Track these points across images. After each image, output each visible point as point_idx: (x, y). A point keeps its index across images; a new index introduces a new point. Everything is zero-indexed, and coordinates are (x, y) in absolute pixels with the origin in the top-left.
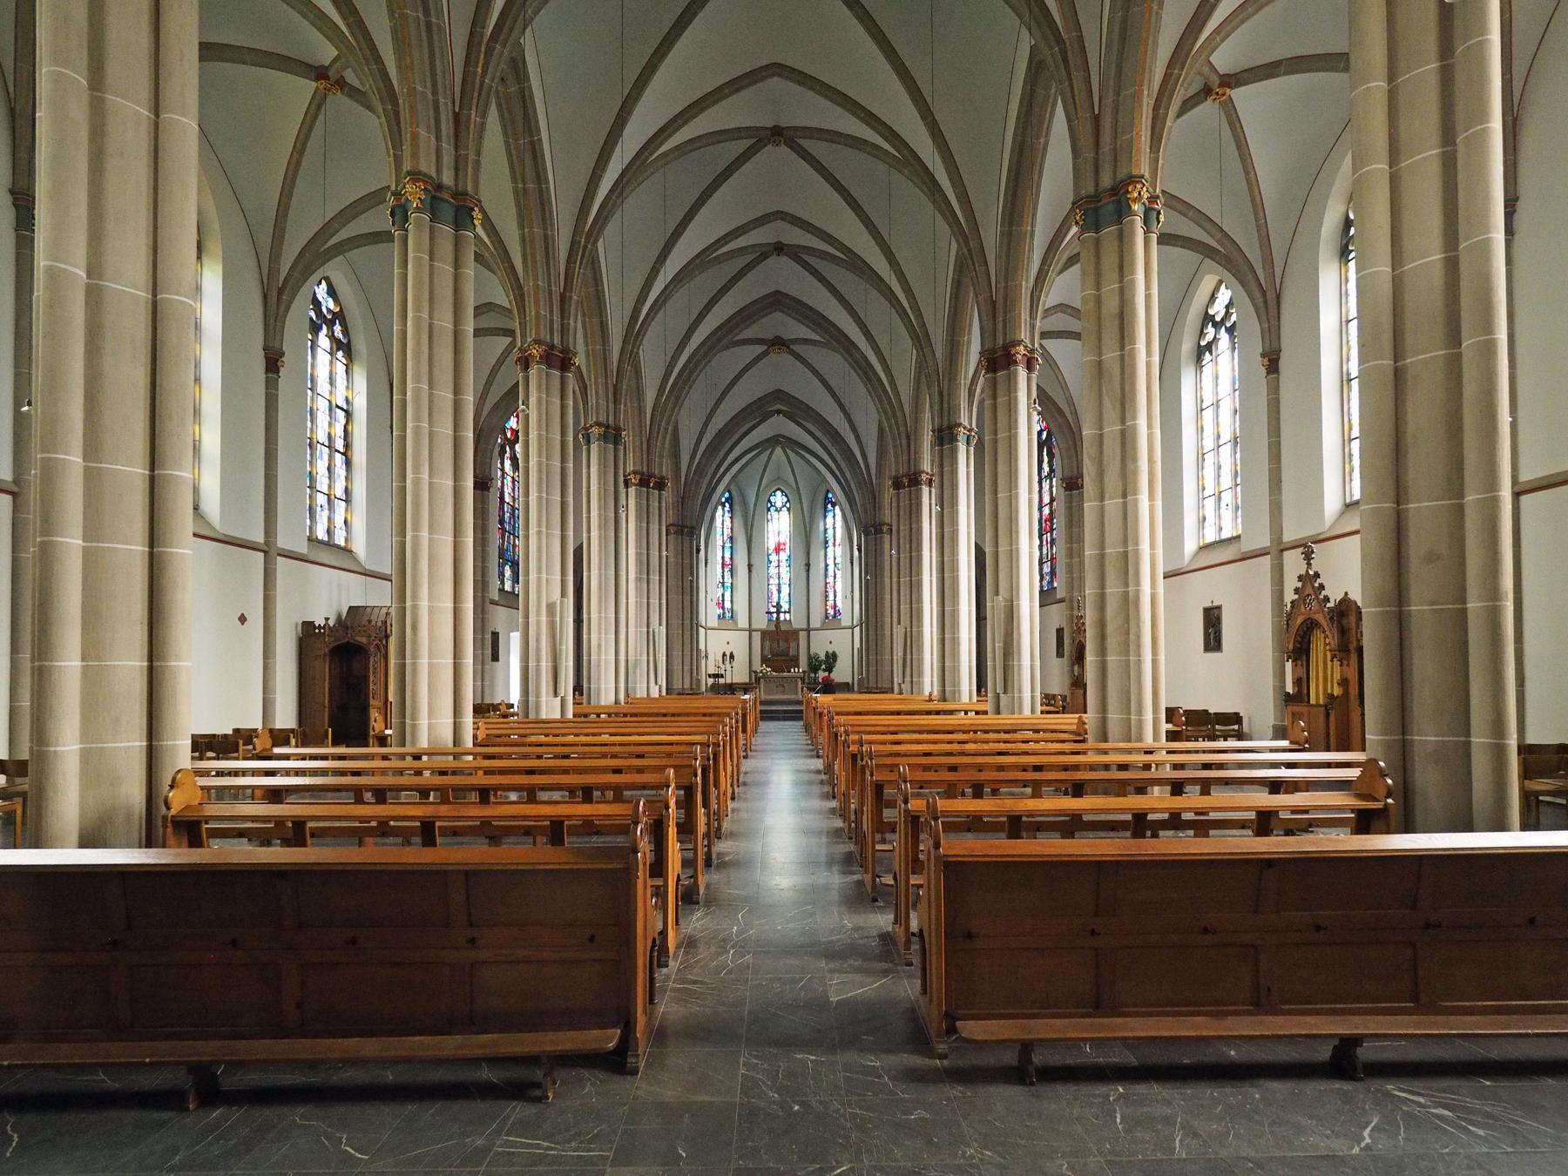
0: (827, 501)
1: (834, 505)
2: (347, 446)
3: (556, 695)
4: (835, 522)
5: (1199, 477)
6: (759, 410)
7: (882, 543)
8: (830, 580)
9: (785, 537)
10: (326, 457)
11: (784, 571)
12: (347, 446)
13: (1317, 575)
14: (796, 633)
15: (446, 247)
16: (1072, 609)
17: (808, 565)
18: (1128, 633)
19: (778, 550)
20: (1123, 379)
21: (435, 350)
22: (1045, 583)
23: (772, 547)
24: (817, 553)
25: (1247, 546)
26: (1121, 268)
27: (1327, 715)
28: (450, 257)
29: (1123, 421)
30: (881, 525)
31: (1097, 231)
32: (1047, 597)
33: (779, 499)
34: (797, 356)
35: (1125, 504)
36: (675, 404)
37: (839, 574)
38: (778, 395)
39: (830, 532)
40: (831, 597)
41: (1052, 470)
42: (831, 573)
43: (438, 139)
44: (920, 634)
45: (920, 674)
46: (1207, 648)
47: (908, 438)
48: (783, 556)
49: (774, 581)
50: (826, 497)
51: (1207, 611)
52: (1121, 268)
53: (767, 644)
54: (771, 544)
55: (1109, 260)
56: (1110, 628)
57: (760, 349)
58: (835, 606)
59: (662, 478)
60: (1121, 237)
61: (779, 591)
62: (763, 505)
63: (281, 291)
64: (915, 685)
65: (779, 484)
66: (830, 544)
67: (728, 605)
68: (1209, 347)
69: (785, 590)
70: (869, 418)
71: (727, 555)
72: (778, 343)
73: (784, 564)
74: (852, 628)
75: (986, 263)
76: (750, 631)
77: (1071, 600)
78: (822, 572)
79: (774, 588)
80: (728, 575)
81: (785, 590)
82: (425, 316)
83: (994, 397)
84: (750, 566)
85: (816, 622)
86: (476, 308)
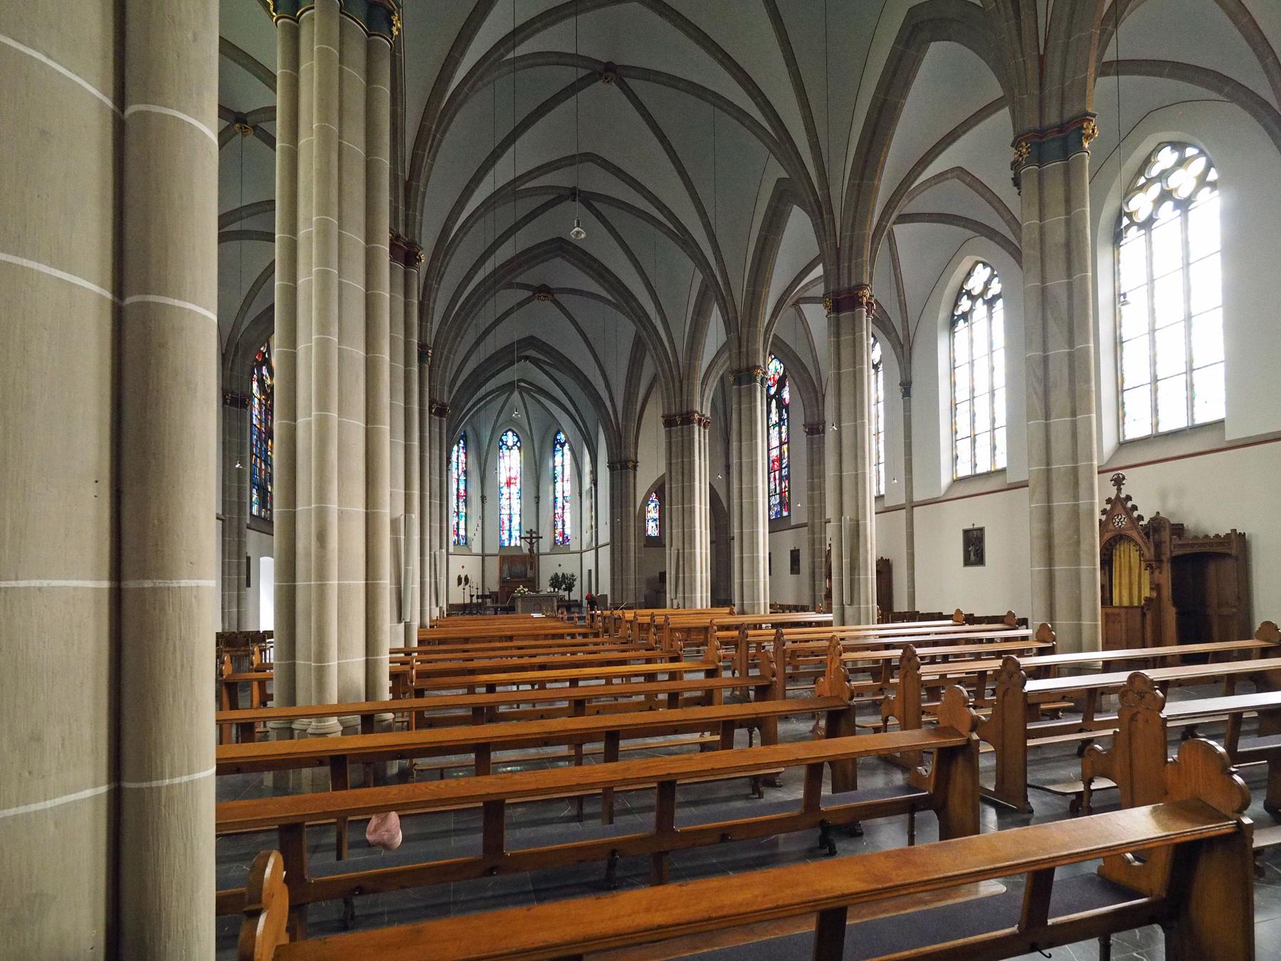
0: (555, 442)
1: (562, 445)
3: (400, 620)
5: (953, 423)
6: (505, 357)
7: (627, 477)
8: (559, 511)
9: (515, 472)
14: (231, 404)
15: (357, 53)
16: (813, 533)
17: (538, 498)
18: (1078, 543)
19: (509, 484)
20: (1070, 305)
21: (345, 177)
22: (773, 513)
24: (546, 487)
25: (1011, 478)
26: (1068, 201)
27: (1144, 615)
28: (361, 62)
29: (1071, 343)
30: (626, 462)
31: (1041, 163)
32: (776, 525)
33: (510, 438)
35: (1074, 425)
36: (457, 335)
37: (567, 505)
38: (531, 342)
39: (559, 469)
40: (560, 526)
41: (781, 419)
42: (559, 504)
44: (692, 555)
45: (693, 590)
46: (967, 562)
47: (681, 382)
49: (505, 512)
50: (555, 439)
51: (966, 533)
52: (1068, 201)
53: (506, 567)
54: (503, 479)
55: (1055, 191)
56: (1058, 540)
57: (528, 293)
58: (563, 534)
59: (443, 405)
60: (1067, 171)
61: (510, 521)
62: (496, 443)
64: (687, 599)
65: (513, 426)
66: (559, 479)
67: (462, 532)
68: (965, 316)
71: (462, 487)
72: (543, 291)
73: (515, 496)
75: (831, 213)
76: (483, 556)
77: (813, 526)
78: (551, 503)
79: (505, 518)
82: (335, 128)
83: (838, 334)
84: (483, 498)
86: (224, 220)
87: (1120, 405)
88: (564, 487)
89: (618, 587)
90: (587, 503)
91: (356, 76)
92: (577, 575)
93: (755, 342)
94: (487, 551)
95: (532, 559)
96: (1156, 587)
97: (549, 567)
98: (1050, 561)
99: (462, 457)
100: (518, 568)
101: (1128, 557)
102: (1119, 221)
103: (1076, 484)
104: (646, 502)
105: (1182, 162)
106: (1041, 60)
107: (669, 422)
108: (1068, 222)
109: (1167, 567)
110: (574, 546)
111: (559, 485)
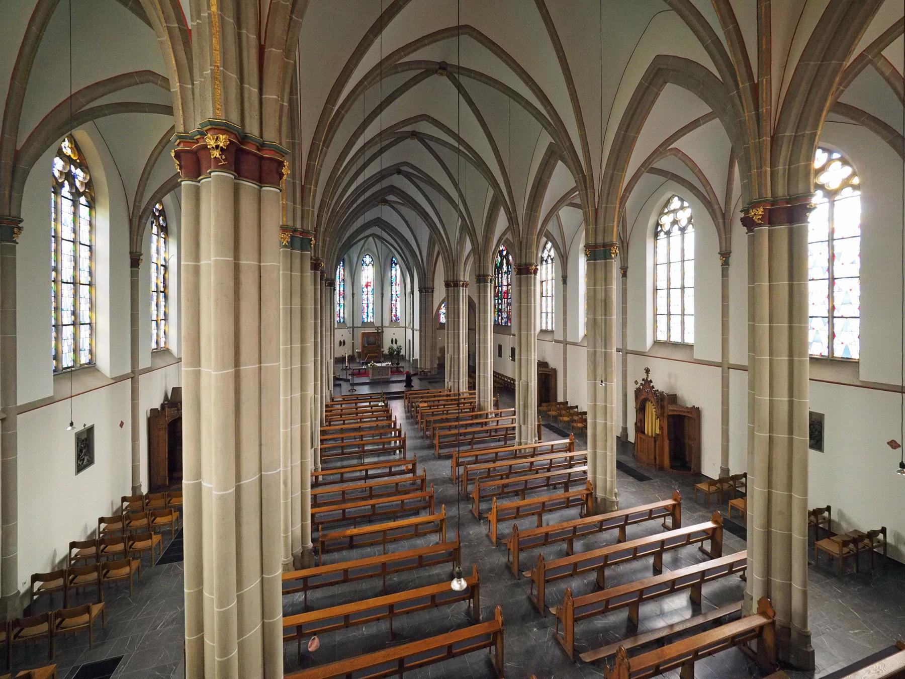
0: (392, 262)
1: (396, 264)
2: (165, 287)
4: (396, 272)
8: (394, 302)
10: (155, 298)
11: (370, 296)
12: (165, 287)
13: (651, 381)
17: (382, 294)
19: (367, 286)
23: (364, 284)
24: (387, 288)
26: (606, 280)
27: (655, 441)
33: (368, 259)
34: (393, 208)
39: (394, 277)
41: (508, 271)
43: (295, 203)
48: (370, 289)
49: (365, 302)
52: (606, 280)
58: (396, 315)
62: (360, 262)
63: (141, 218)
67: (342, 315)
69: (371, 306)
70: (424, 234)
71: (342, 289)
73: (370, 293)
74: (405, 328)
79: (365, 305)
80: (342, 299)
81: (371, 306)
83: (520, 286)
84: (353, 294)
85: (386, 323)
87: (655, 321)
88: (397, 289)
89: (423, 356)
90: (408, 299)
91: (297, 274)
92: (403, 346)
93: (488, 262)
94: (355, 325)
95: (379, 335)
96: (661, 428)
97: (389, 335)
98: (237, 363)
99: (342, 272)
100: (372, 339)
101: (651, 410)
102: (657, 228)
103: (606, 414)
104: (439, 308)
105: (682, 208)
106: (596, 210)
107: (447, 285)
108: (606, 290)
109: (666, 420)
110: (402, 324)
111: (394, 287)
